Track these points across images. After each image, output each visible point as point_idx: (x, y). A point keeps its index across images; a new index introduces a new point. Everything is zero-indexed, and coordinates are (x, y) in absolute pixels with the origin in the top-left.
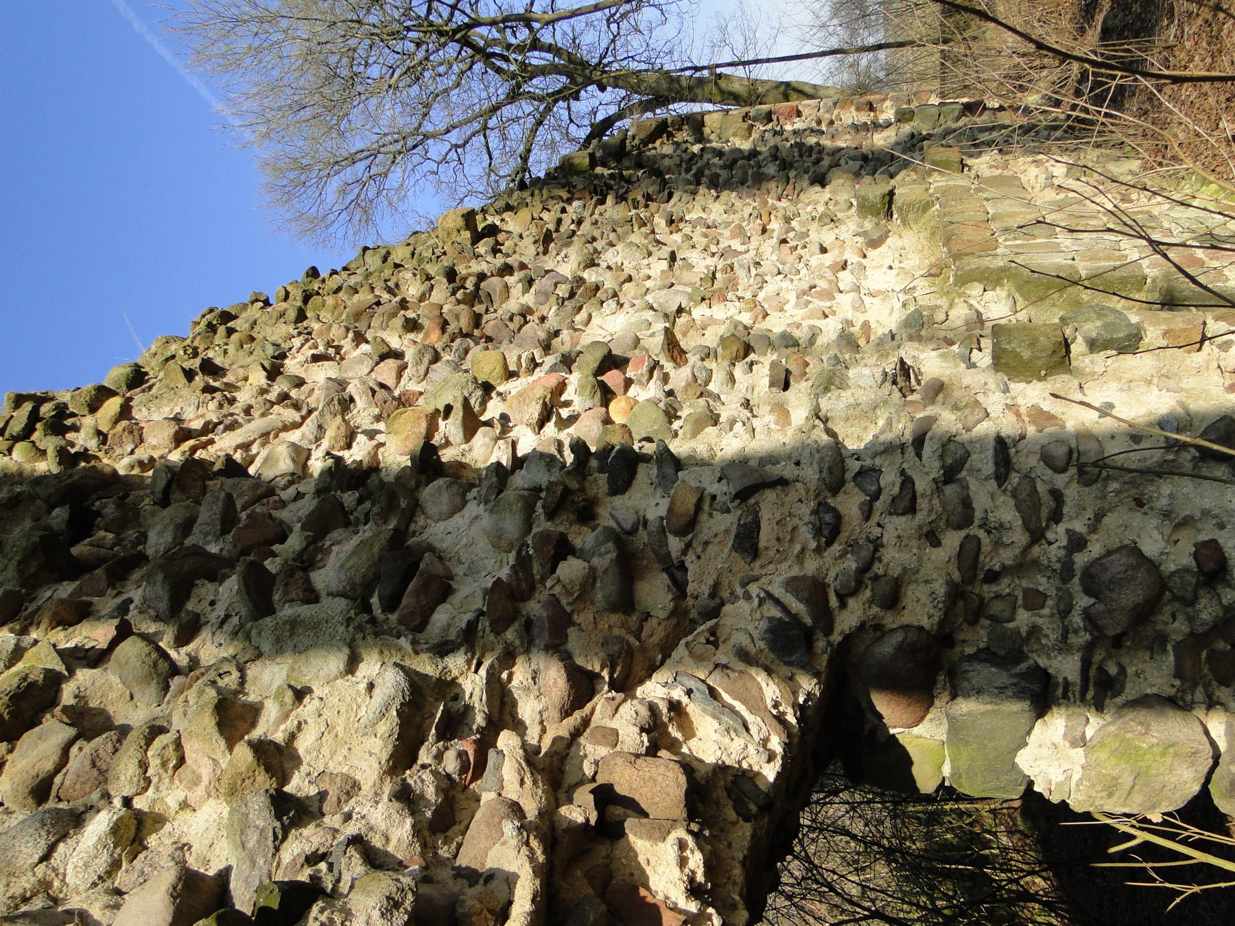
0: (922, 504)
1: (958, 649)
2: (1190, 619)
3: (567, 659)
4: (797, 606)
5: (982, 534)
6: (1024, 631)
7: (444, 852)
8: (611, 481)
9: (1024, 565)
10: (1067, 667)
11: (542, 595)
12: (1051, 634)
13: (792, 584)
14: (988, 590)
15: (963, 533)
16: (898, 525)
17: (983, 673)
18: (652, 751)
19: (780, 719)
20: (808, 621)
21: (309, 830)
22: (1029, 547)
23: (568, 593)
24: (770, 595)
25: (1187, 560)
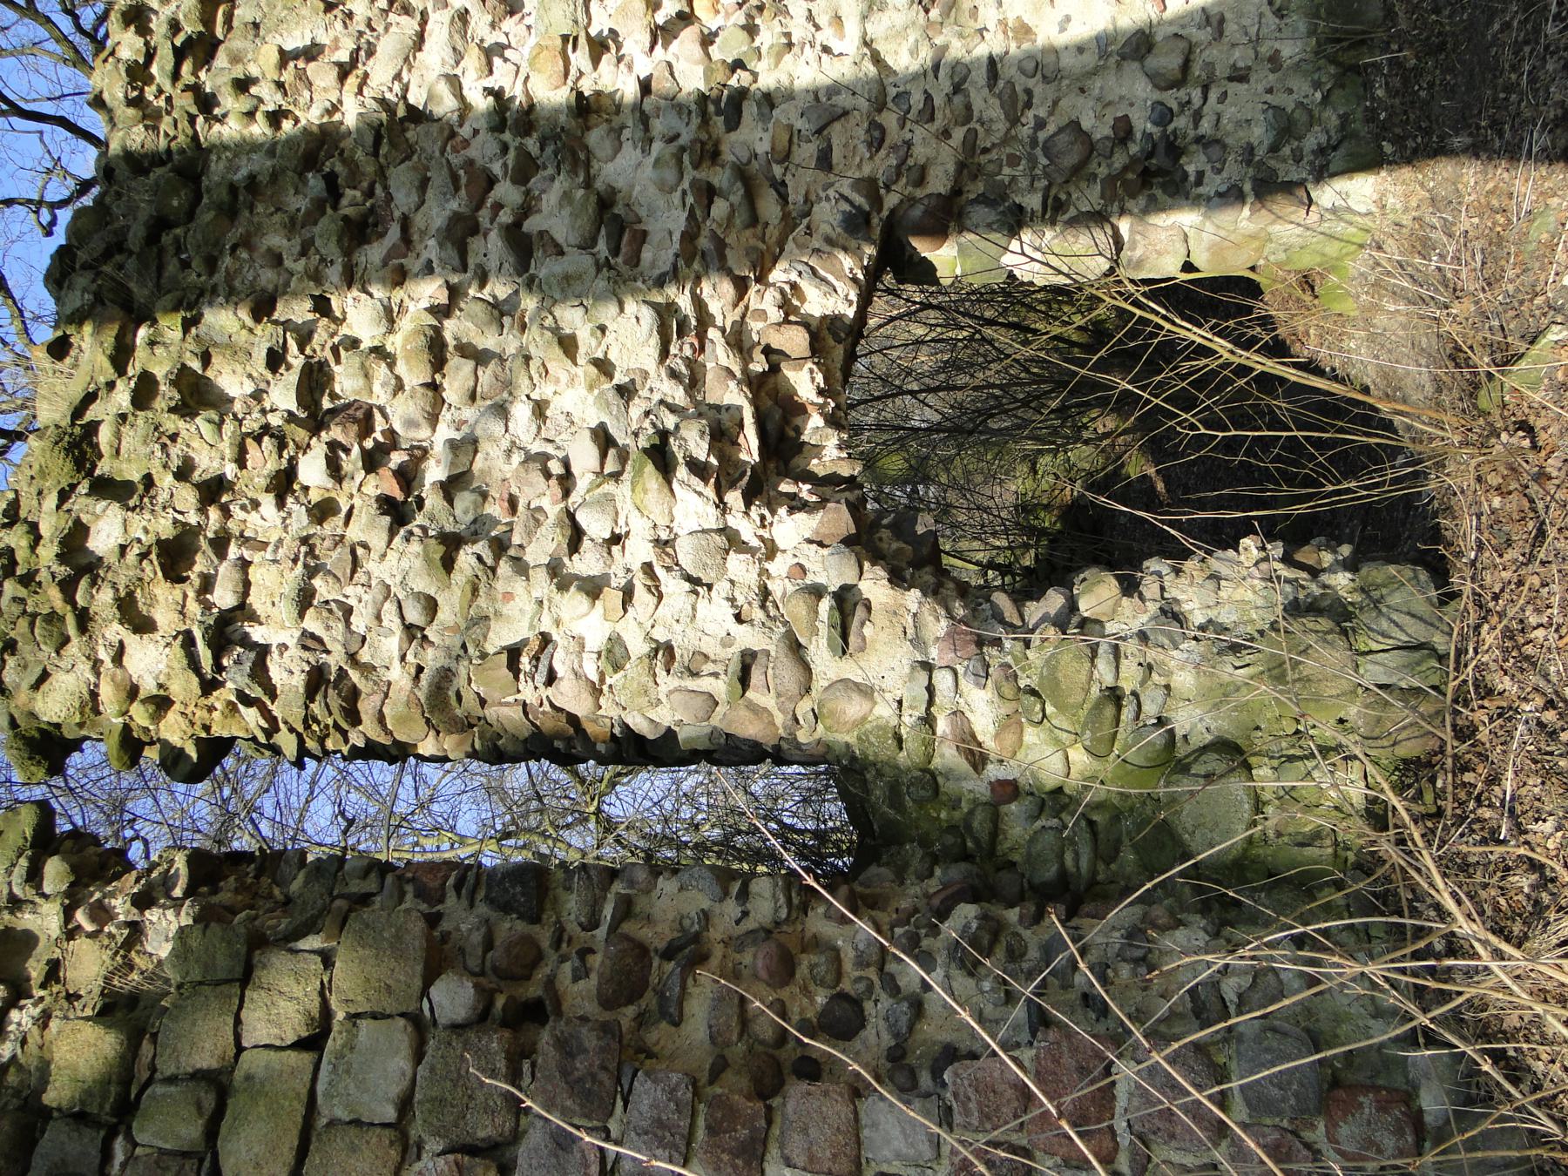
0: (938, 115)
1: (964, 197)
2: (1109, 166)
3: (729, 273)
4: (859, 199)
5: (978, 127)
6: (1007, 180)
7: (699, 398)
8: (727, 122)
9: (1007, 140)
10: (1033, 202)
11: (705, 232)
12: (1024, 183)
13: (858, 184)
14: (983, 159)
15: (965, 128)
16: (919, 133)
17: (980, 213)
18: (786, 321)
19: (854, 280)
20: (867, 208)
21: (636, 400)
22: (1009, 130)
23: (720, 225)
24: (842, 196)
25: (1108, 131)
